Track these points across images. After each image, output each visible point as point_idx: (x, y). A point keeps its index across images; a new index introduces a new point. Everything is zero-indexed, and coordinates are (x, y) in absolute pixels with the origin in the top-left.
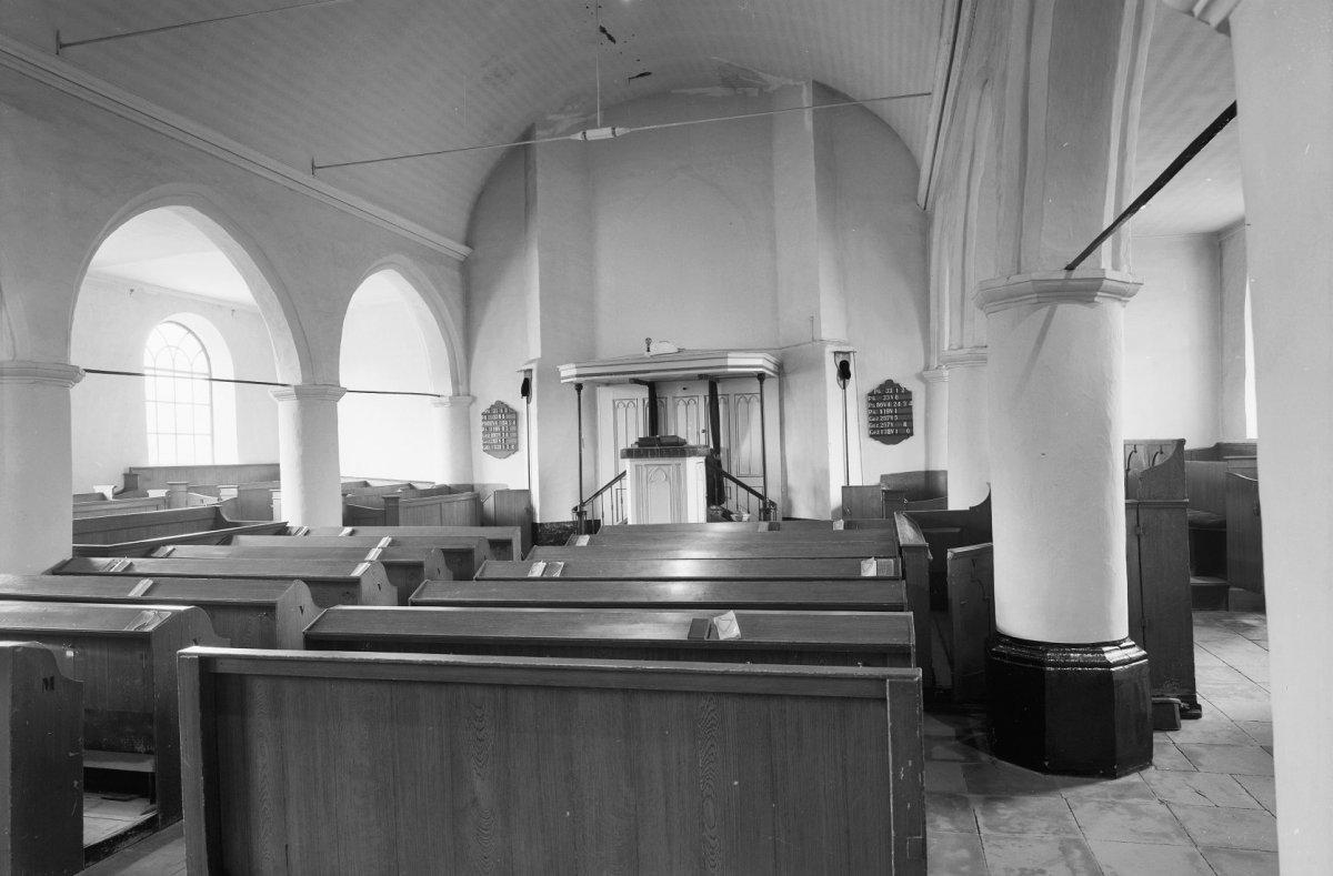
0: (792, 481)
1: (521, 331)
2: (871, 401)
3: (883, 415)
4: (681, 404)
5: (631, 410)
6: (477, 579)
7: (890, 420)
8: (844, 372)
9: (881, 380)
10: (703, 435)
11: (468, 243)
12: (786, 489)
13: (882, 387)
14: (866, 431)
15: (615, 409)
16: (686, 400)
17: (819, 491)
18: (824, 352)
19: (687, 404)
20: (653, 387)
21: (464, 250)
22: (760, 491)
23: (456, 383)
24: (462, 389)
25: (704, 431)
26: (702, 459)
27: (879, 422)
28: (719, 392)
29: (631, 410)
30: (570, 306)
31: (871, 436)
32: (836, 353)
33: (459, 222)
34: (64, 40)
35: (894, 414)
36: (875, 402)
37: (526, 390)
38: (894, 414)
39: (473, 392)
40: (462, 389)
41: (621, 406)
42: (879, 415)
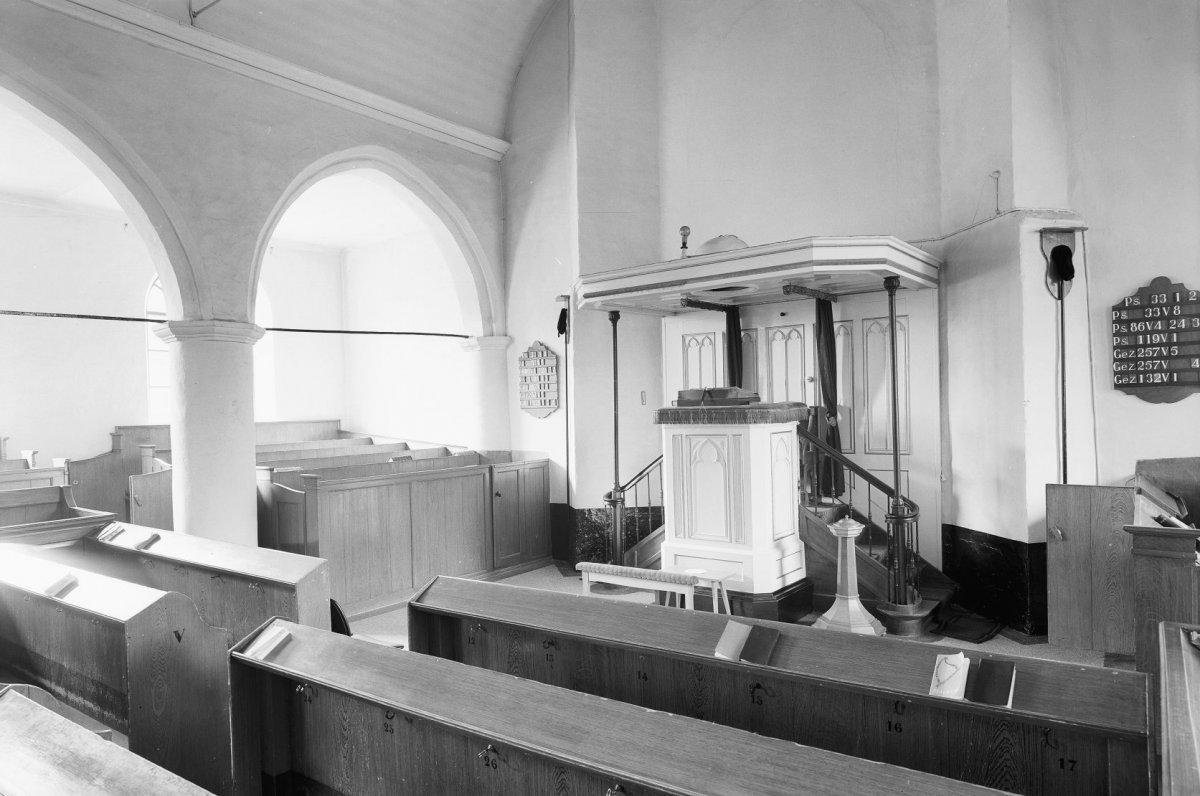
0: (958, 464)
1: (556, 256)
2: (1118, 321)
3: (1145, 346)
4: (777, 328)
5: (707, 350)
6: (527, 779)
7: (1160, 357)
8: (1061, 266)
9: (1144, 278)
10: (810, 387)
11: (506, 136)
12: (948, 478)
13: (1143, 293)
14: (1106, 377)
15: (685, 348)
16: (786, 331)
17: (1008, 484)
18: (1017, 233)
19: (787, 338)
20: (733, 314)
21: (499, 145)
22: (892, 485)
23: (488, 319)
24: (497, 327)
25: (812, 380)
26: (793, 426)
27: (1136, 360)
28: (836, 315)
29: (707, 350)
30: (625, 184)
31: (1117, 387)
32: (1043, 232)
33: (491, 108)
34: (195, 9)
35: (1169, 344)
36: (1128, 322)
37: (562, 327)
38: (1169, 344)
39: (511, 332)
40: (497, 327)
41: (779, 336)
42: (1136, 347)
